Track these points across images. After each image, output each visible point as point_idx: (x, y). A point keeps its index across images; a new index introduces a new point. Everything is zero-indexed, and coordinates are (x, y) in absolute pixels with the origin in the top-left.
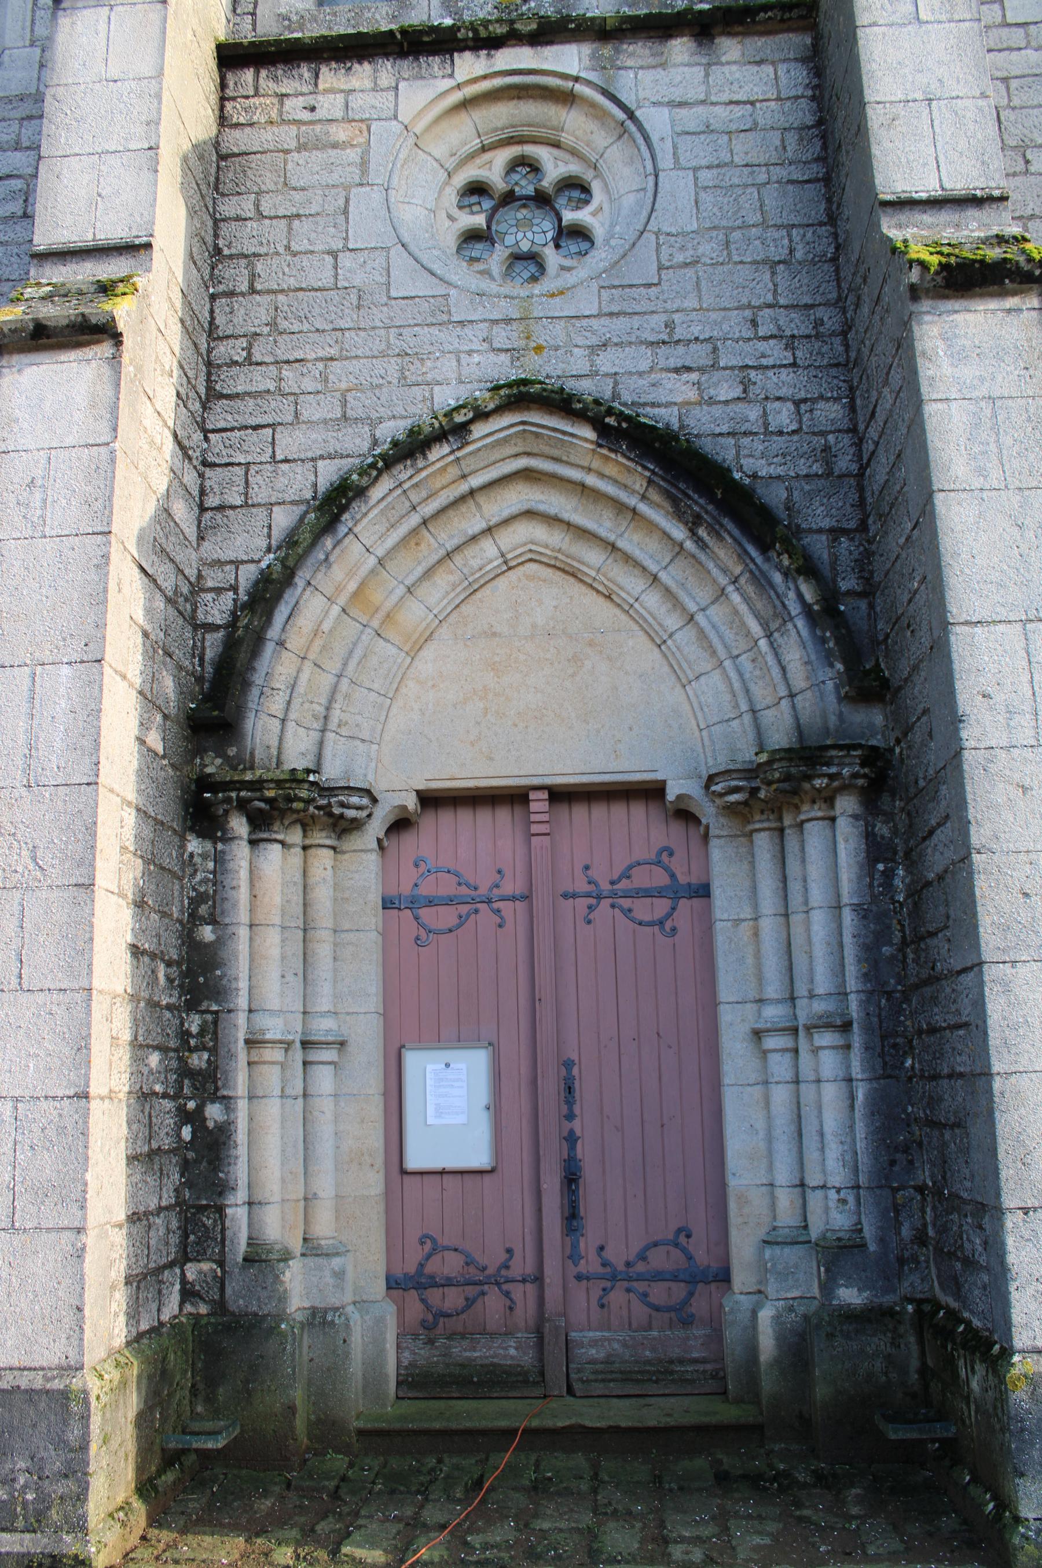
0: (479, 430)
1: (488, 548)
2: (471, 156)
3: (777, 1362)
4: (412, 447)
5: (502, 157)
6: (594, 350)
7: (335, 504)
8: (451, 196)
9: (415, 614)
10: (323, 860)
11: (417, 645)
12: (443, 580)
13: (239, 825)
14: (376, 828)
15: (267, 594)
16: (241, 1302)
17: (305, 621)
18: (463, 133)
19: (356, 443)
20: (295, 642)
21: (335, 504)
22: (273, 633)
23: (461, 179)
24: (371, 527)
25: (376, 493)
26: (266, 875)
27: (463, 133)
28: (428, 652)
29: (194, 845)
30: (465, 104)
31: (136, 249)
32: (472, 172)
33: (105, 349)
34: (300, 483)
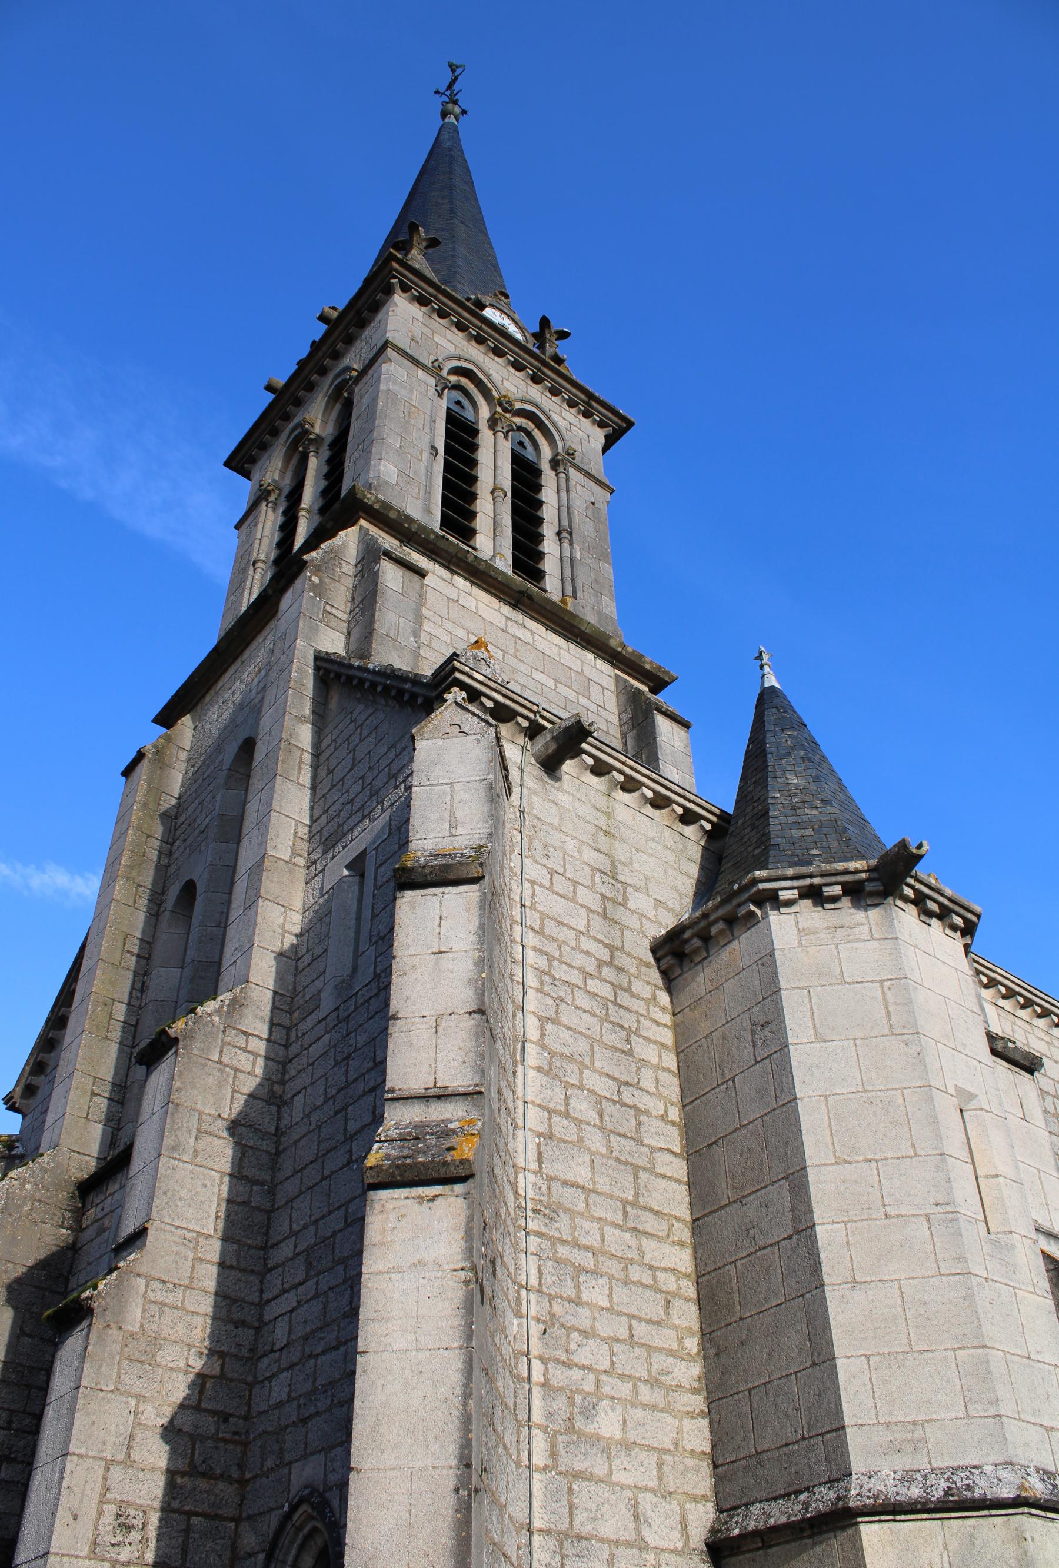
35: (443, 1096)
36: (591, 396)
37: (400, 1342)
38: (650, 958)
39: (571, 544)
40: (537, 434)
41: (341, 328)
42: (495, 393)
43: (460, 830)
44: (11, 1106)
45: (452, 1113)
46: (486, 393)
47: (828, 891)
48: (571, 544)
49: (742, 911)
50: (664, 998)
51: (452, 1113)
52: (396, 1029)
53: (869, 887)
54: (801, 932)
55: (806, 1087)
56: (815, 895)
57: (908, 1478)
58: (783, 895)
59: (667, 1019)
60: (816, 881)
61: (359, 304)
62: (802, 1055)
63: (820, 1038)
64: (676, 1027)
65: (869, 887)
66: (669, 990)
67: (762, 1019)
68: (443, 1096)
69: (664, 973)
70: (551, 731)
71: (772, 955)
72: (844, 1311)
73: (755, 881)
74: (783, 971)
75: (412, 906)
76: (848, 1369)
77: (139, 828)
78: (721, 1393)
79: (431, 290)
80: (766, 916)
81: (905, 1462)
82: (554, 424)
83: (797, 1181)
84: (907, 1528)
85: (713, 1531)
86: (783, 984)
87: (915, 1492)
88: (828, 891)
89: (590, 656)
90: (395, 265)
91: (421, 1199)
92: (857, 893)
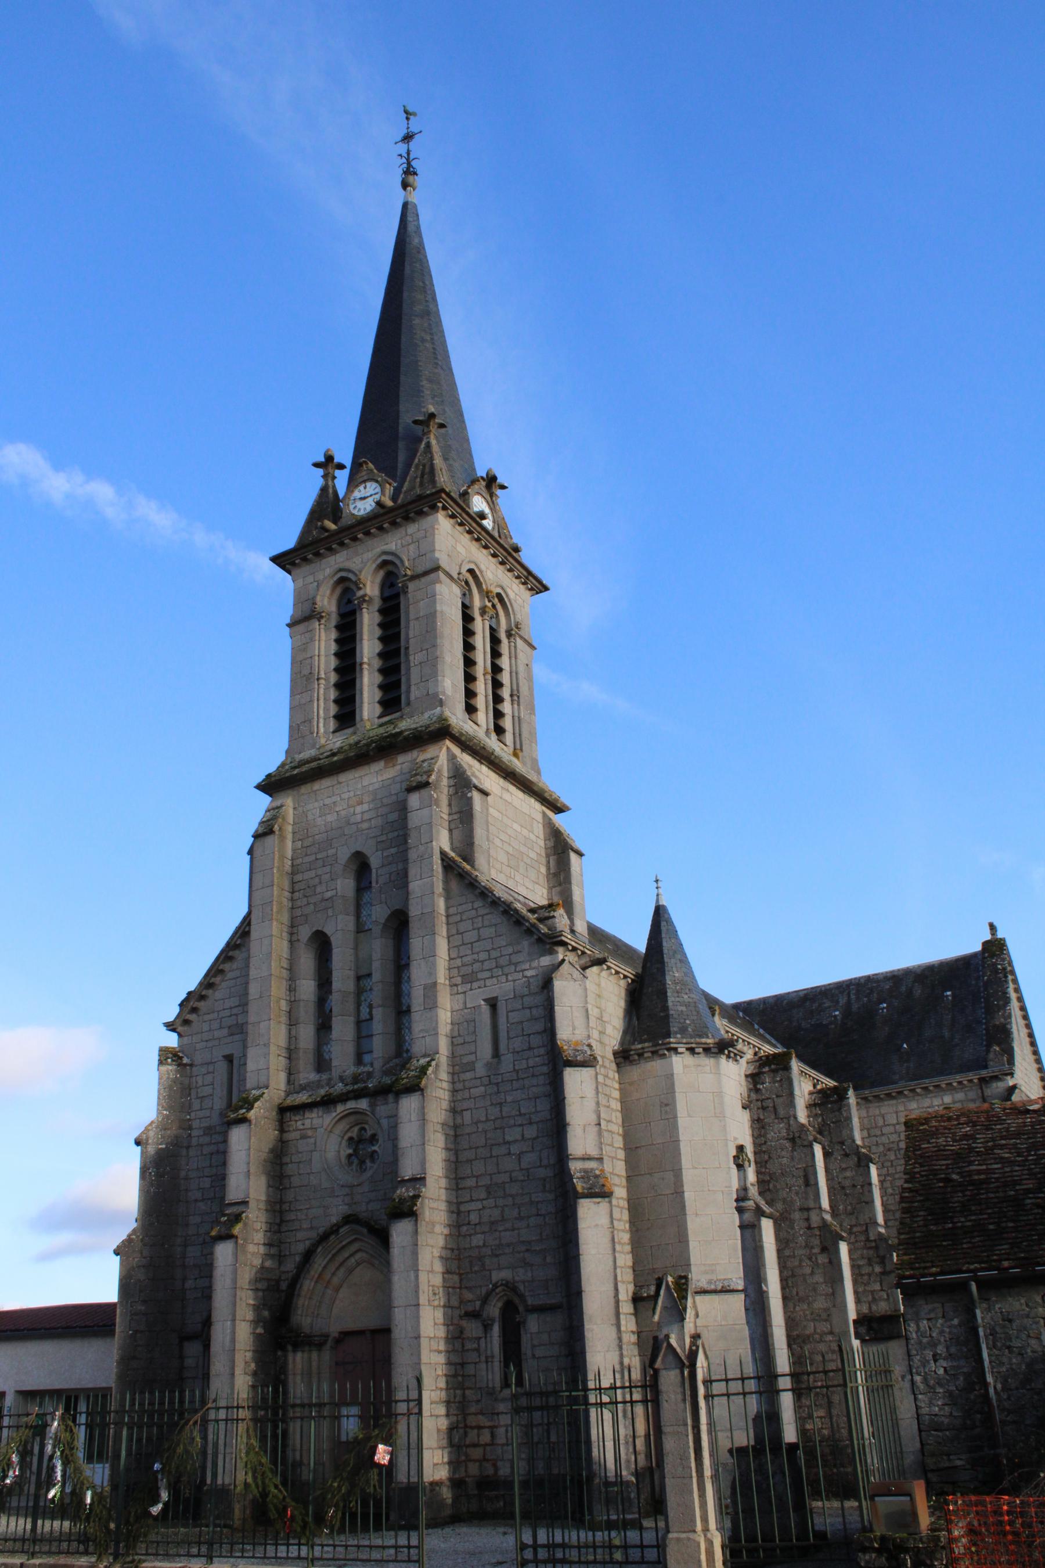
0: (341, 1230)
1: (353, 1260)
2: (348, 1130)
3: (791, 1059)
4: (324, 1238)
5: (356, 1129)
6: (368, 1203)
7: (308, 1256)
8: (344, 1143)
9: (336, 1281)
10: (315, 1355)
11: (337, 1290)
12: (342, 1270)
13: (290, 1348)
14: (329, 1343)
15: (295, 1281)
16: (688, 1022)
17: (305, 1288)
18: (343, 1126)
19: (314, 1235)
20: (303, 1293)
21: (308, 1256)
22: (296, 1293)
23: (346, 1137)
24: (319, 1262)
25: (319, 1250)
26: (297, 1361)
27: (343, 1126)
28: (341, 1290)
29: (279, 1353)
30: (336, 1122)
31: (245, 1203)
32: (349, 1134)
33: (233, 1240)
34: (301, 1248)
35: (590, 1159)
36: (530, 573)
37: (593, 1252)
38: (612, 1058)
39: (519, 705)
40: (499, 606)
41: (391, 515)
42: (484, 587)
43: (577, 1032)
44: (170, 1026)
45: (592, 1165)
46: (478, 584)
47: (697, 1050)
48: (519, 705)
49: (661, 1052)
50: (617, 1075)
51: (592, 1165)
52: (570, 1129)
53: (714, 1050)
54: (685, 1067)
55: (683, 1136)
56: (692, 1051)
57: (710, 1282)
58: (680, 1050)
59: (617, 1086)
60: (693, 1045)
61: (410, 507)
62: (682, 1121)
63: (689, 1116)
64: (620, 1090)
65: (714, 1050)
66: (618, 1072)
67: (665, 1102)
68: (590, 1159)
69: (618, 1065)
70: (589, 956)
71: (672, 1075)
72: (693, 1225)
73: (670, 1043)
74: (677, 1083)
75: (570, 1074)
76: (693, 1244)
77: (278, 886)
78: (637, 1245)
79: (459, 511)
80: (670, 1057)
81: (709, 1277)
82: (510, 600)
83: (678, 1174)
84: (707, 1298)
85: (634, 1293)
86: (677, 1090)
87: (713, 1287)
88: (697, 1050)
89: (533, 800)
90: (443, 495)
91: (595, 1203)
92: (707, 1050)
